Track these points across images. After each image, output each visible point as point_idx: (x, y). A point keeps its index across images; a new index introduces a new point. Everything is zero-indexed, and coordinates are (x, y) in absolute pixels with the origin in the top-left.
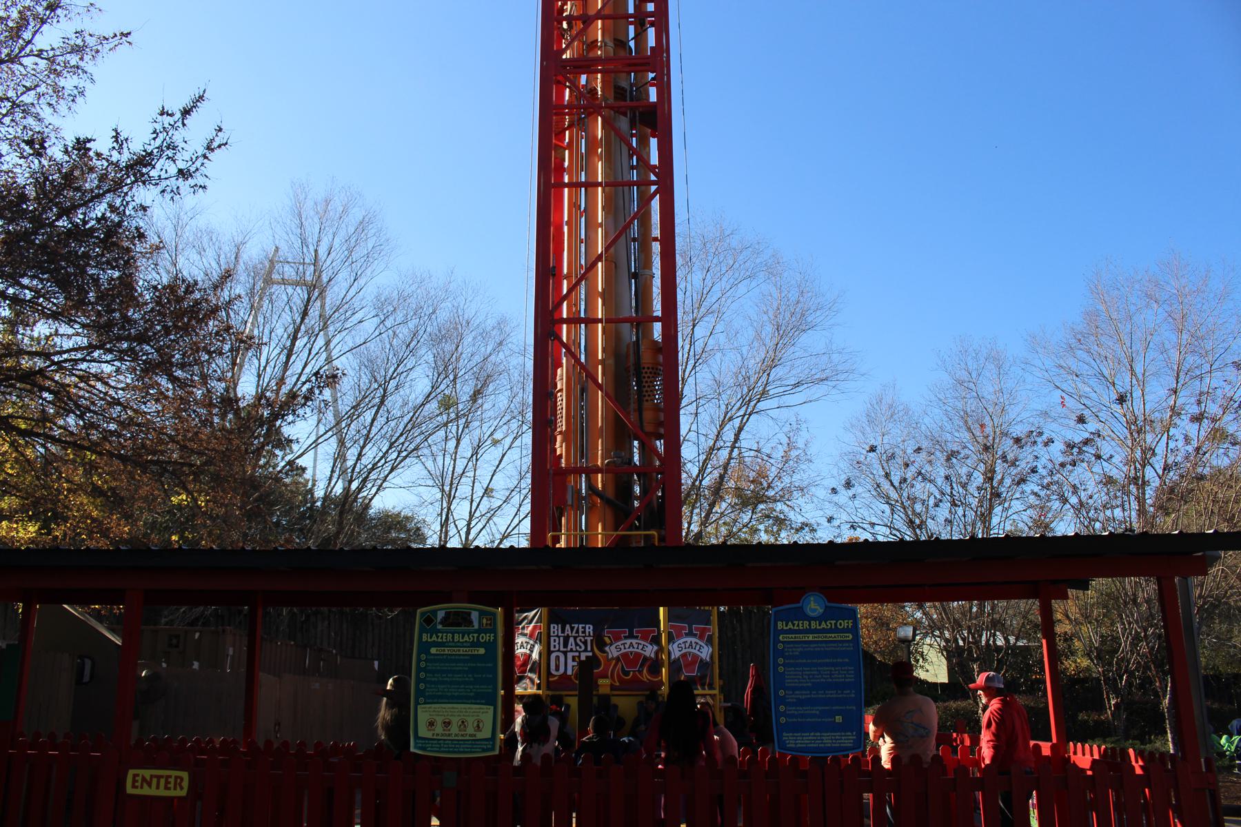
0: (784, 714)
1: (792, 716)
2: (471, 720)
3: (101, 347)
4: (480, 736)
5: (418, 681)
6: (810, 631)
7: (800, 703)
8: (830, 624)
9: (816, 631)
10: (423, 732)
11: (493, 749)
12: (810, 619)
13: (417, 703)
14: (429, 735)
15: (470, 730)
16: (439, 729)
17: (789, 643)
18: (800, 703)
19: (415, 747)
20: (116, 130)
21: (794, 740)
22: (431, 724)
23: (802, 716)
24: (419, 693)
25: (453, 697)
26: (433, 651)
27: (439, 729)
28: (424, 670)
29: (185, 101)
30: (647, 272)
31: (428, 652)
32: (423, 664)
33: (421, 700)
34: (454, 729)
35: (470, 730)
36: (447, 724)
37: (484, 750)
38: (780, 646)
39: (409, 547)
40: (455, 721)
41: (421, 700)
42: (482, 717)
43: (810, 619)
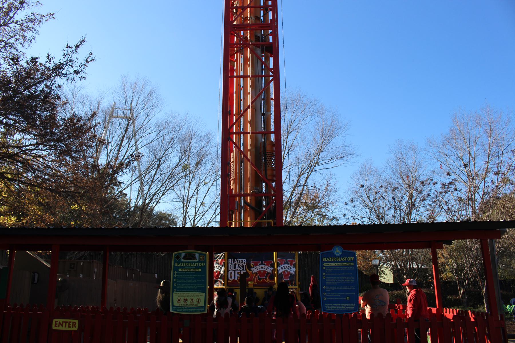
0: (325, 296)
1: (329, 297)
2: (195, 299)
3: (42, 144)
4: (199, 305)
5: (174, 282)
6: (336, 262)
7: (332, 291)
8: (344, 259)
9: (339, 262)
10: (176, 304)
11: (205, 311)
12: (336, 257)
13: (173, 292)
14: (178, 305)
15: (195, 303)
16: (182, 302)
17: (327, 266)
18: (332, 291)
19: (172, 310)
22: (179, 300)
23: (333, 297)
24: (174, 287)
25: (188, 289)
26: (180, 270)
27: (182, 302)
28: (176, 278)
29: (77, 42)
30: (268, 113)
31: (177, 271)
32: (175, 276)
33: (175, 290)
34: (188, 302)
35: (195, 303)
36: (186, 300)
37: (201, 311)
38: (324, 268)
40: (189, 299)
41: (175, 290)
42: (200, 297)
43: (336, 257)
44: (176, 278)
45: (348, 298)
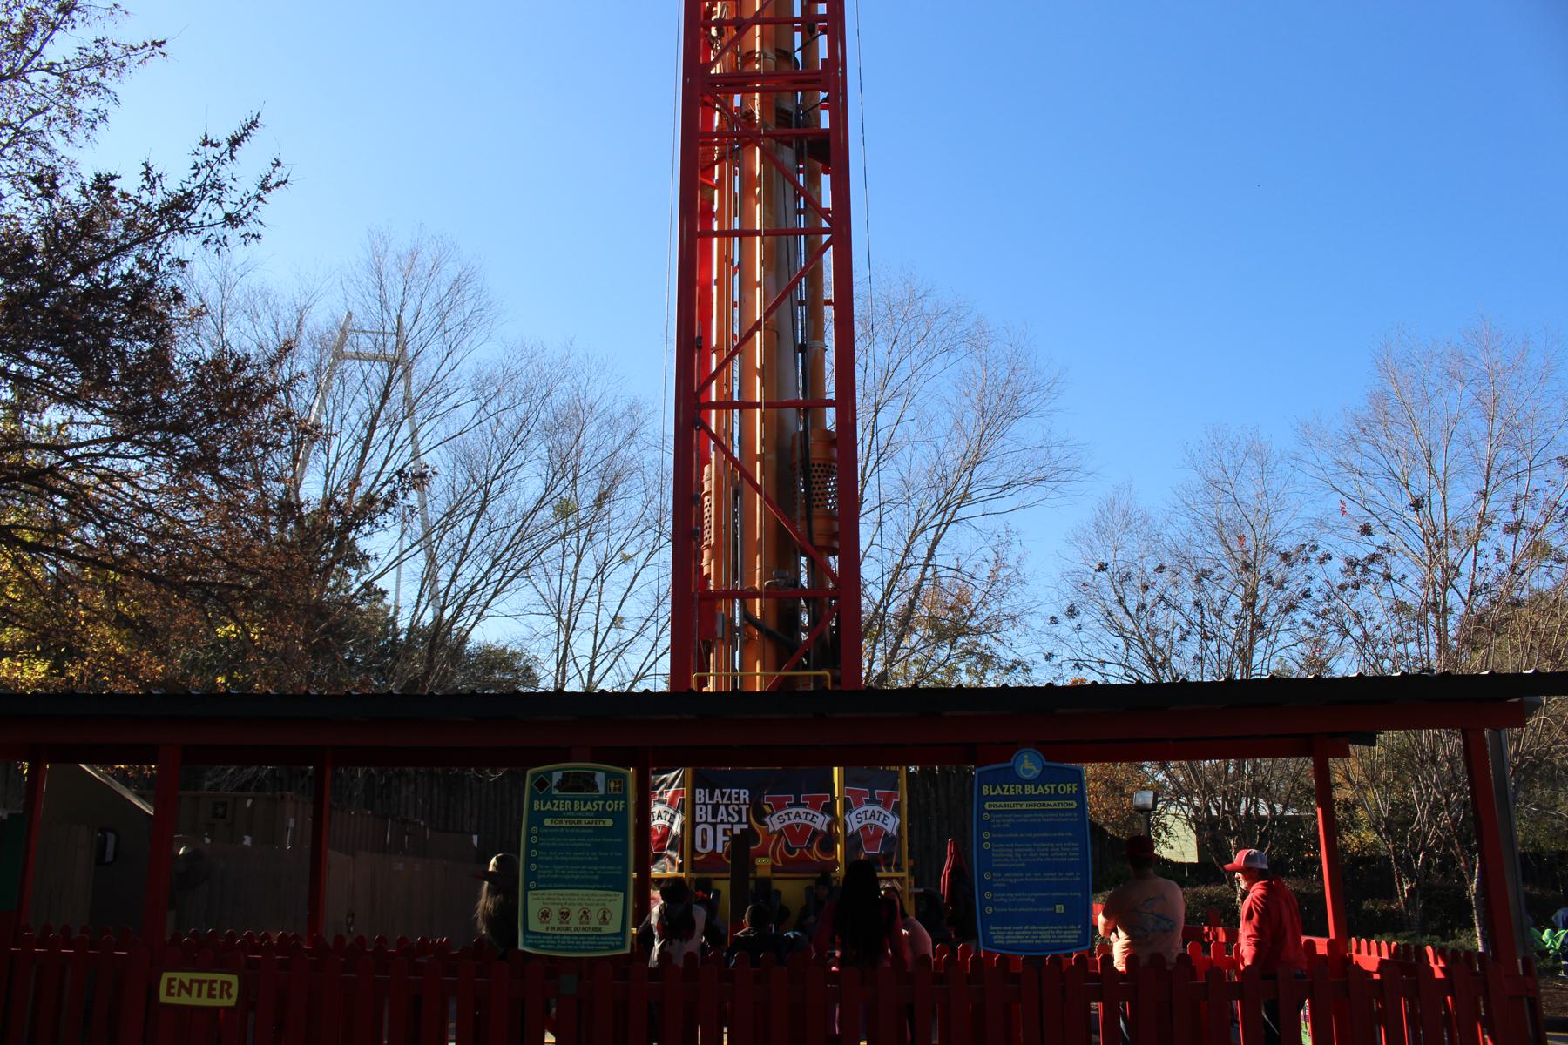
0: (991, 902)
1: (1001, 905)
2: (595, 910)
3: (127, 438)
4: (606, 929)
5: (529, 860)
6: (1023, 797)
7: (1011, 888)
8: (1049, 788)
9: (1031, 798)
10: (535, 925)
11: (623, 946)
12: (1023, 782)
13: (527, 889)
14: (542, 929)
15: (594, 923)
16: (555, 921)
17: (997, 812)
18: (1011, 888)
19: (525, 944)
20: (146, 165)
21: (1003, 935)
22: (545, 915)
23: (1014, 904)
24: (530, 875)
25: (572, 881)
26: (547, 822)
27: (555, 921)
28: (536, 846)
29: (234, 128)
31: (540, 824)
32: (534, 840)
33: (532, 884)
34: (574, 922)
35: (594, 923)
36: (565, 915)
37: (612, 948)
38: (986, 817)
39: (517, 692)
40: (575, 910)
41: (532, 884)
42: (609, 906)
43: (1023, 782)
44: (536, 846)
45: (1060, 908)
